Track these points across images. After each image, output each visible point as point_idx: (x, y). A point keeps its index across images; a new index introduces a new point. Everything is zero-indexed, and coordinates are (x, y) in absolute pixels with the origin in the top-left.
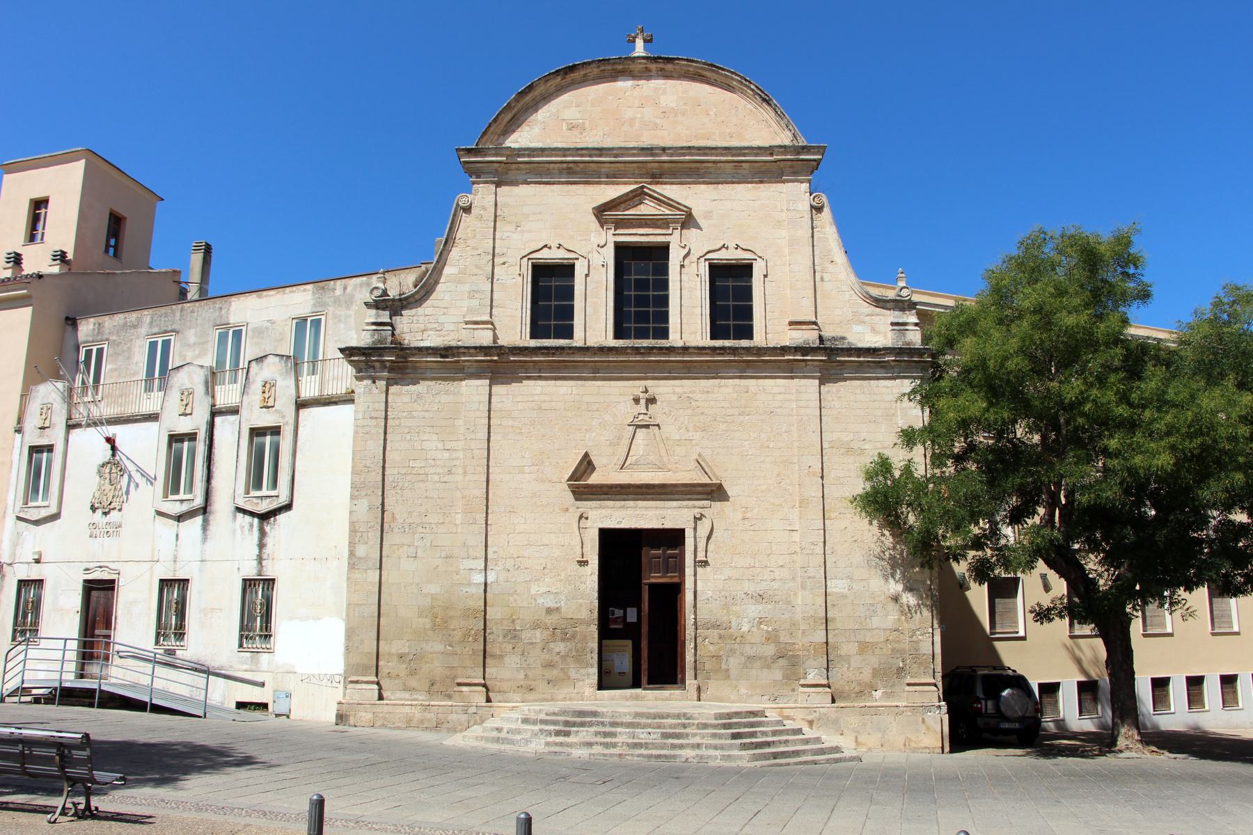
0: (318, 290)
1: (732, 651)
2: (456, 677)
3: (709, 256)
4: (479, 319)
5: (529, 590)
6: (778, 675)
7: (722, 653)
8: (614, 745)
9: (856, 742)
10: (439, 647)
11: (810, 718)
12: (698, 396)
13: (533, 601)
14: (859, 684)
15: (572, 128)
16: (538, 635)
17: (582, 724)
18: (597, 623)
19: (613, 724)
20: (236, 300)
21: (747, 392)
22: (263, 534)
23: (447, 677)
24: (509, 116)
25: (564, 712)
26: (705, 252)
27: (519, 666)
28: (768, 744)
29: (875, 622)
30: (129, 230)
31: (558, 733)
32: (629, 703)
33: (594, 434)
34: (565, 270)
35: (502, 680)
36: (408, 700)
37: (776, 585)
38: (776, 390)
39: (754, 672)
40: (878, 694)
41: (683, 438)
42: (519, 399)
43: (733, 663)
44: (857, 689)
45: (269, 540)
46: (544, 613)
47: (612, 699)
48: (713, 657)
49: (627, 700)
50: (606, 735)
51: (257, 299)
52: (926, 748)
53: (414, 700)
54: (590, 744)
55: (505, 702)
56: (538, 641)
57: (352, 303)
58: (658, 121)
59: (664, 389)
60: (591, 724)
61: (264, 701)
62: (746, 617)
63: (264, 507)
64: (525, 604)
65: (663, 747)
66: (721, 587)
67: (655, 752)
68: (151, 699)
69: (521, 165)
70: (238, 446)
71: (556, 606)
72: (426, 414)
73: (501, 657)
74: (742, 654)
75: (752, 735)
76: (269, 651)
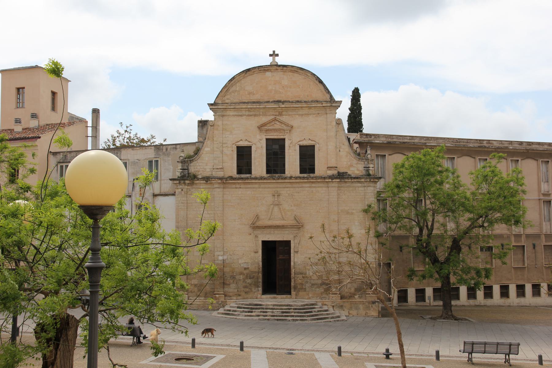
1: (307, 282)
2: (214, 292)
3: (299, 143)
4: (218, 167)
8: (266, 316)
11: (333, 305)
14: (350, 293)
15: (250, 93)
16: (241, 277)
17: (256, 309)
19: (267, 309)
21: (312, 192)
24: (226, 89)
25: (250, 305)
28: (316, 315)
30: (59, 97)
31: (249, 312)
32: (272, 300)
35: (230, 292)
40: (357, 297)
44: (350, 295)
46: (243, 269)
49: (272, 299)
50: (264, 312)
51: (132, 151)
53: (200, 300)
54: (258, 316)
58: (281, 90)
60: (259, 309)
64: (237, 266)
65: (282, 316)
70: (132, 210)
71: (247, 267)
73: (229, 284)
75: (311, 312)
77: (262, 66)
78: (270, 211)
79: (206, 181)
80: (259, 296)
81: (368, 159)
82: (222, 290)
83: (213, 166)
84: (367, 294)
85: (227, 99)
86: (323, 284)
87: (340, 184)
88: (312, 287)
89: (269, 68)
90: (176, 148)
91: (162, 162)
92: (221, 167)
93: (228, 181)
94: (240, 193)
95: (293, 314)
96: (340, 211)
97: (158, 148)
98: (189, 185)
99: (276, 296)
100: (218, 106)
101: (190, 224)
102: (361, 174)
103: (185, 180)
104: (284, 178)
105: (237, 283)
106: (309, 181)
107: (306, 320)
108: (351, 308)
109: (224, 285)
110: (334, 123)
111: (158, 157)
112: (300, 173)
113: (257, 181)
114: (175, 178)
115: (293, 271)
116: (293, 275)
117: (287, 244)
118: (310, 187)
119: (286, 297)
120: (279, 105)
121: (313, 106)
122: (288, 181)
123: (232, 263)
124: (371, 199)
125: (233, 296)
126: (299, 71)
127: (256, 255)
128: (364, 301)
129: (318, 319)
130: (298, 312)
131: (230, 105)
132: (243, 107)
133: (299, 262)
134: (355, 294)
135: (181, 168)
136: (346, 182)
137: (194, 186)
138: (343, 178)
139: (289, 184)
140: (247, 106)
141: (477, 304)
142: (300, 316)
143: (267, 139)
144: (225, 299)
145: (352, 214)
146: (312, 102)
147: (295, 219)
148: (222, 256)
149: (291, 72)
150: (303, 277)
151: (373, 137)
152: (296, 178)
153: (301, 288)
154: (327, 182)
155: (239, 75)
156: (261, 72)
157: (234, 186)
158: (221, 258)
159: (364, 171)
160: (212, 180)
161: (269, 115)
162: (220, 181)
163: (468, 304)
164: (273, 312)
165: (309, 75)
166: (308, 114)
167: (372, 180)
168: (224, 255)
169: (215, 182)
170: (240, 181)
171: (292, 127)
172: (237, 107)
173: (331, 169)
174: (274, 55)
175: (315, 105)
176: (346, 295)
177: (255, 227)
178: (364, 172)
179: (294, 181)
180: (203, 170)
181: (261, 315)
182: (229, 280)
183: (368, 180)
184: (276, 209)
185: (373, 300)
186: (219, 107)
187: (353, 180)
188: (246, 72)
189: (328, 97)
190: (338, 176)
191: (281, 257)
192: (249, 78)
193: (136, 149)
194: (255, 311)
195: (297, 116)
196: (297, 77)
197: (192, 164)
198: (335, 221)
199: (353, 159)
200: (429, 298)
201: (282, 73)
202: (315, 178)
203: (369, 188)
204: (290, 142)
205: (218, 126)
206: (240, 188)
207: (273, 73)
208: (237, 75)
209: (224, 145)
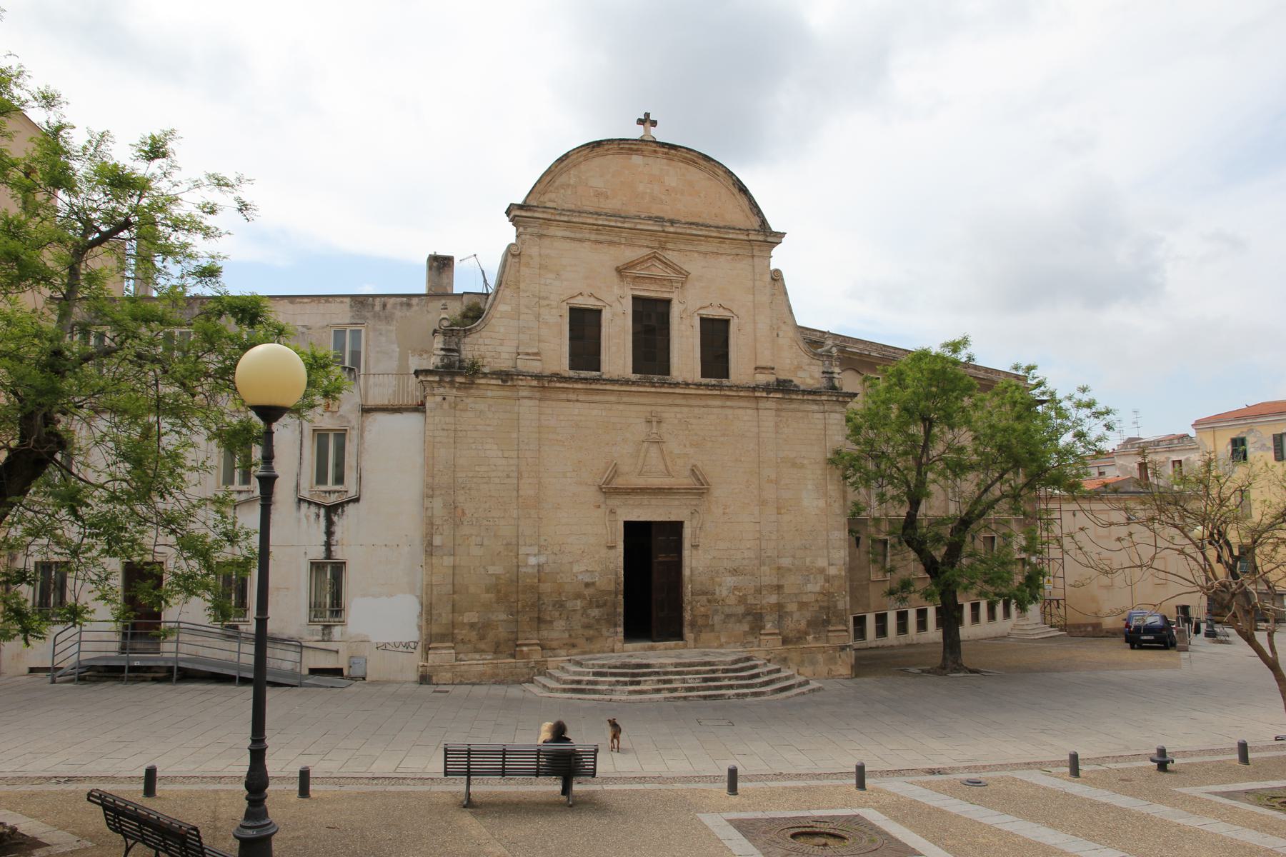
1: (717, 611)
2: (517, 639)
3: (701, 312)
4: (530, 351)
6: (746, 627)
10: (503, 616)
11: (768, 657)
15: (598, 195)
17: (644, 675)
22: (330, 523)
23: (509, 640)
24: (549, 178)
25: (624, 666)
26: (698, 307)
29: (810, 587)
31: (632, 683)
35: (552, 640)
37: (745, 562)
38: (746, 418)
39: (730, 625)
40: (810, 638)
42: (562, 418)
43: (717, 619)
44: (797, 635)
45: (338, 529)
57: (392, 319)
58: (663, 197)
59: (673, 414)
61: (339, 666)
62: (726, 586)
63: (333, 499)
64: (569, 580)
67: (701, 693)
68: (128, 662)
72: (489, 429)
73: (551, 622)
74: (722, 613)
76: (343, 623)
77: (628, 140)
78: (642, 455)
79: (503, 381)
80: (618, 646)
81: (832, 357)
82: (535, 636)
83: (518, 347)
84: (829, 631)
85: (550, 201)
86: (748, 614)
87: (781, 404)
88: (727, 620)
89: (640, 147)
90: (409, 305)
91: (371, 334)
92: (535, 350)
93: (553, 385)
94: (576, 411)
95: (726, 682)
96: (779, 461)
97: (362, 302)
98: (462, 387)
99: (650, 643)
100: (535, 211)
101: (460, 480)
102: (818, 386)
103: (453, 374)
104: (674, 384)
105: (568, 618)
106: (723, 393)
107: (763, 693)
108: (801, 663)
109: (539, 623)
110: (768, 278)
111: (359, 322)
112: (703, 376)
113: (616, 388)
114: (427, 368)
115: (688, 588)
116: (687, 597)
117: (677, 527)
118: (722, 407)
119: (676, 644)
120: (662, 226)
121: (731, 236)
122: (682, 391)
123: (558, 573)
124: (837, 437)
125: (561, 648)
126: (701, 162)
127: (612, 553)
128: (825, 645)
130: (737, 678)
131: (560, 214)
133: (701, 569)
135: (441, 346)
136: (791, 400)
137: (472, 391)
138: (788, 391)
139: (681, 397)
140: (596, 219)
141: (909, 642)
143: (635, 298)
144: (542, 657)
145: (802, 466)
148: (535, 555)
149: (682, 162)
150: (709, 601)
154: (756, 397)
155: (578, 152)
156: (622, 154)
157: (563, 396)
158: (532, 561)
159: (824, 379)
160: (517, 379)
161: (640, 246)
162: (535, 383)
164: (684, 681)
165: (720, 172)
166: (718, 254)
167: (841, 399)
168: (539, 553)
169: (524, 383)
170: (580, 386)
171: (687, 275)
172: (574, 220)
173: (763, 371)
174: (646, 121)
176: (790, 635)
177: (610, 491)
180: (493, 354)
181: (664, 689)
182: (551, 611)
183: (834, 399)
184: (654, 451)
186: (536, 215)
187: (805, 397)
188: (593, 147)
190: (777, 386)
191: (662, 558)
192: (597, 162)
193: (300, 303)
194: (646, 681)
195: (696, 255)
196: (696, 175)
197: (467, 340)
198: (772, 481)
199: (803, 354)
201: (665, 160)
202: (735, 389)
203: (833, 415)
204: (682, 307)
205: (531, 257)
206: (577, 401)
207: (646, 158)
208: (574, 149)
209: (543, 302)
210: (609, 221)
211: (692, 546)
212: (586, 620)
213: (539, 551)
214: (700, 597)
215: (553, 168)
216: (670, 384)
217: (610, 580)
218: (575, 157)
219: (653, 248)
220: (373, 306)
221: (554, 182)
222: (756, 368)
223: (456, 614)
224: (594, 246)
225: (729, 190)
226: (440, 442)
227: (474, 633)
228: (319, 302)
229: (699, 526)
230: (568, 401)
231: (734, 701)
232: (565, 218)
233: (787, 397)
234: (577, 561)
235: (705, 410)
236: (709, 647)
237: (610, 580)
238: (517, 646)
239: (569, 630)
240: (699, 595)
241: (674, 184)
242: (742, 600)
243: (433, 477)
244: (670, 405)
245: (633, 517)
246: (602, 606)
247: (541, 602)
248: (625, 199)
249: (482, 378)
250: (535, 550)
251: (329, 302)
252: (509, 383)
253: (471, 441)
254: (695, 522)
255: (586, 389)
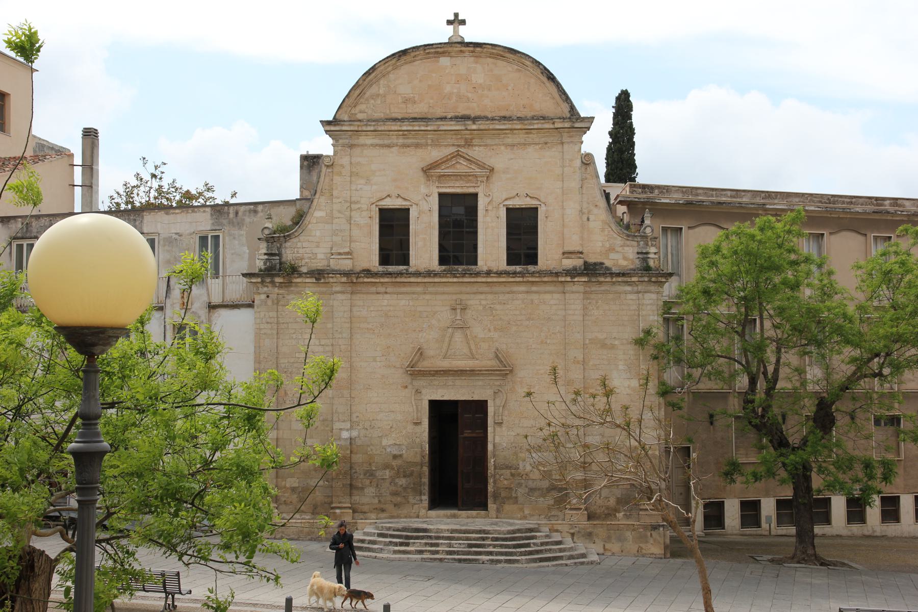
0: (215, 213)
1: (520, 485)
2: (332, 503)
3: (507, 203)
4: (342, 251)
5: (381, 442)
7: (512, 486)
9: (604, 548)
11: (572, 531)
12: (498, 307)
13: (384, 450)
15: (406, 101)
16: (387, 473)
17: (417, 538)
18: (427, 465)
19: (438, 538)
20: (147, 214)
24: (358, 92)
25: (404, 529)
26: (503, 199)
27: (374, 494)
31: (401, 544)
33: (425, 334)
34: (404, 213)
35: (363, 504)
36: (299, 519)
38: (552, 302)
40: (620, 515)
41: (487, 336)
43: (521, 491)
46: (391, 458)
47: (438, 517)
48: (506, 488)
51: (165, 215)
52: (653, 554)
54: (421, 552)
55: (366, 519)
56: (387, 477)
57: (243, 225)
58: (470, 95)
59: (476, 302)
60: (422, 538)
64: (378, 452)
65: (469, 553)
66: (512, 441)
69: (368, 133)
73: (362, 489)
75: (528, 545)
77: (432, 45)
78: (447, 340)
79: (316, 279)
80: (423, 512)
81: (646, 237)
83: (332, 248)
84: (641, 510)
88: (530, 494)
89: (446, 49)
90: (255, 212)
92: (347, 250)
93: (361, 280)
95: (491, 549)
96: (587, 342)
97: (219, 211)
99: (456, 512)
100: (342, 125)
101: (283, 366)
103: (273, 276)
104: (475, 274)
108: (608, 539)
110: (578, 163)
111: (218, 228)
112: (508, 264)
113: (419, 280)
115: (491, 462)
116: (491, 470)
117: (480, 407)
119: (478, 514)
120: (465, 125)
121: (536, 126)
122: (484, 280)
123: (368, 446)
124: (651, 318)
125: (371, 512)
126: (508, 55)
127: (418, 429)
128: (635, 523)
129: (541, 560)
130: (501, 546)
131: (366, 125)
132: (393, 128)
133: (505, 444)
134: (616, 510)
135: (265, 251)
136: (601, 283)
137: (292, 289)
139: (485, 285)
141: (866, 533)
142: (506, 554)
143: (441, 195)
144: (353, 519)
145: (613, 347)
146: (533, 118)
147: (497, 357)
148: (347, 430)
149: (490, 57)
150: (512, 475)
151: (656, 191)
152: (500, 274)
153: (507, 497)
157: (373, 289)
160: (328, 277)
162: (344, 279)
163: (849, 533)
164: (450, 545)
165: (528, 63)
166: (525, 144)
167: (653, 279)
168: (352, 428)
169: (335, 280)
170: (386, 280)
171: (492, 170)
173: (570, 256)
174: (456, 21)
175: (540, 126)
176: (598, 511)
178: (638, 263)
179: (495, 280)
180: (310, 255)
181: (426, 551)
183: (646, 279)
184: (458, 336)
185: (653, 521)
187: (614, 279)
189: (565, 108)
191: (467, 433)
194: (414, 543)
196: (503, 69)
197: (288, 244)
199: (615, 236)
200: (769, 518)
201: (473, 58)
203: (647, 296)
204: (487, 200)
205: (342, 166)
206: (386, 293)
207: (454, 59)
208: (380, 62)
209: (354, 206)
210: (413, 126)
211: (495, 423)
212: (394, 488)
213: (351, 426)
214: (503, 471)
215: (361, 82)
216: (471, 274)
217: (416, 453)
218: (382, 68)
219: (458, 146)
220: (228, 213)
221: (365, 94)
222: (564, 253)
223: (279, 480)
224: (402, 150)
225: (539, 78)
226: (265, 334)
227: (295, 496)
228: (187, 213)
229: (502, 405)
230: (378, 293)
231: (488, 566)
232: (372, 128)
233: (594, 280)
234: (386, 435)
235: (511, 295)
236: (513, 518)
237: (416, 453)
238: (333, 508)
239: (378, 497)
240: (503, 469)
241: (481, 81)
242: (546, 475)
243: (259, 363)
244: (475, 293)
245: (437, 397)
246: (409, 476)
247: (353, 471)
248: (431, 101)
249: (298, 277)
250: (348, 425)
251: (196, 212)
252: (322, 281)
253: (293, 331)
254: (498, 402)
255: (392, 282)
